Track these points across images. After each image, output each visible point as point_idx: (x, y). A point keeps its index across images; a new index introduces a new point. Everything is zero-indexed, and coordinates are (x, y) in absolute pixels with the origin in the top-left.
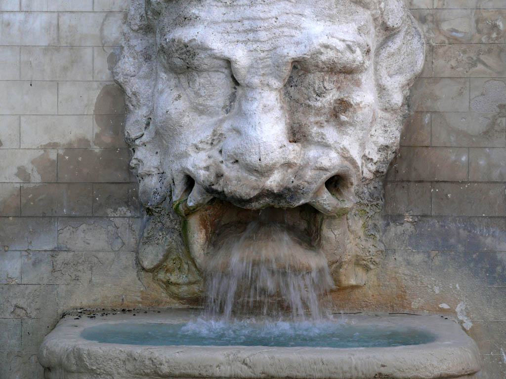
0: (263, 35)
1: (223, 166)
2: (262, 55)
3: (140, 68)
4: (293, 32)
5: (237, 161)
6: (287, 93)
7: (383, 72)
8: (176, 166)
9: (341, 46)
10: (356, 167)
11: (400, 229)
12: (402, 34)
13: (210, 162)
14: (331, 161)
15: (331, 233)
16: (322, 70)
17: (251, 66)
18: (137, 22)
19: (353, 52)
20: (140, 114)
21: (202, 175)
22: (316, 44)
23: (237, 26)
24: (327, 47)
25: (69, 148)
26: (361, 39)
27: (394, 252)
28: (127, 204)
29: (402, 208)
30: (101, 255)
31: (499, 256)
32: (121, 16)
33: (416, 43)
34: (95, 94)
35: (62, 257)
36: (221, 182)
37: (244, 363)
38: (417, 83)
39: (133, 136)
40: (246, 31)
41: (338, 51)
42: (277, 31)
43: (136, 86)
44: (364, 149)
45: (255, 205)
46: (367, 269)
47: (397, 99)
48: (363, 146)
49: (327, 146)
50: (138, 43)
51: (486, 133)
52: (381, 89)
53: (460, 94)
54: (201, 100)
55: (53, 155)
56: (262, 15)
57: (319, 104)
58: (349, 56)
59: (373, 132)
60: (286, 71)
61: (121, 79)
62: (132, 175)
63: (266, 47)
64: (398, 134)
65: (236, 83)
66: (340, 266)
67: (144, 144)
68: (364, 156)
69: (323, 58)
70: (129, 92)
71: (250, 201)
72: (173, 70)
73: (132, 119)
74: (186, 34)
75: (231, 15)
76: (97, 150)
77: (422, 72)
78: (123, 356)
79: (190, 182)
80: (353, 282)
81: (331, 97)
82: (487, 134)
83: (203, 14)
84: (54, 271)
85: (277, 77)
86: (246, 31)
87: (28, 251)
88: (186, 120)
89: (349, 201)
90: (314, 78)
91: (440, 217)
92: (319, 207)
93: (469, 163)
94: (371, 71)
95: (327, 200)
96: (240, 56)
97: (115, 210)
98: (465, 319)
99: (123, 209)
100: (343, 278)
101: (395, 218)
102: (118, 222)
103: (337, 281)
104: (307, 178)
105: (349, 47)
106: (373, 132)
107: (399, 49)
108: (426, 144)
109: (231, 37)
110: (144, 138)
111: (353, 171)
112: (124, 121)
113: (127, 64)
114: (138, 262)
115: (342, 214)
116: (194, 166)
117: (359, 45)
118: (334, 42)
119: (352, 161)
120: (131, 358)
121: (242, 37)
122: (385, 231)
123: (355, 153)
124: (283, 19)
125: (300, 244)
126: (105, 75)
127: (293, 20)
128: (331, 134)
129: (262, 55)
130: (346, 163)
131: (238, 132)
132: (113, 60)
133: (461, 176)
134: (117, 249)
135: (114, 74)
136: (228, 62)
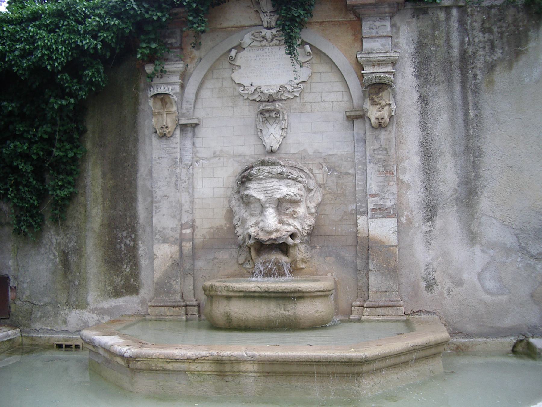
0: (269, 192)
1: (259, 232)
2: (269, 198)
3: (237, 203)
4: (278, 191)
5: (263, 230)
6: (278, 209)
7: (308, 202)
8: (246, 232)
9: (292, 194)
10: (300, 231)
11: (315, 250)
12: (314, 191)
13: (255, 230)
14: (291, 229)
15: (292, 251)
16: (287, 202)
17: (266, 201)
18: (236, 190)
19: (297, 196)
20: (237, 217)
21: (253, 234)
22: (284, 194)
23: (261, 189)
24: (287, 194)
25: (217, 228)
26: (299, 192)
27: (314, 257)
28: (234, 244)
29: (316, 244)
30: (227, 260)
31: (346, 258)
32: (232, 188)
33: (319, 194)
34: (224, 212)
35: (216, 261)
36: (258, 235)
37: (259, 287)
38: (319, 205)
39: (235, 224)
40: (264, 191)
41: (291, 196)
42: (273, 190)
43: (236, 209)
44: (302, 226)
45: (268, 243)
46: (306, 263)
47: (313, 210)
48: (302, 225)
49: (290, 225)
50: (237, 196)
51: (341, 220)
52: (308, 208)
53: (332, 208)
54: (253, 212)
55: (212, 231)
56: (269, 186)
57: (287, 212)
58: (295, 198)
59: (305, 221)
60: (277, 202)
61: (232, 207)
62: (236, 236)
63: (270, 195)
64: (314, 221)
65: (263, 207)
66: (297, 262)
67: (238, 226)
68: (303, 228)
69: (287, 198)
70: (234, 211)
71: (266, 241)
72: (244, 203)
73: (235, 219)
74: (246, 193)
75: (260, 186)
76: (225, 228)
77: (321, 202)
78: (224, 286)
79: (250, 236)
80: (301, 267)
81: (291, 210)
82: (341, 220)
83: (252, 186)
84: (213, 265)
85: (275, 205)
86: (264, 191)
87: (206, 259)
88: (248, 218)
89: (298, 241)
90: (285, 205)
91: (327, 246)
92: (288, 243)
93: (336, 230)
94: (304, 202)
95: (290, 241)
96: (262, 197)
97: (231, 246)
98: (336, 277)
99: (233, 246)
100: (298, 265)
101: (314, 247)
102: (232, 250)
103: (296, 266)
104: (283, 234)
105: (295, 195)
106: (305, 221)
107: (313, 195)
108: (323, 224)
109: (259, 193)
110: (238, 225)
111: (298, 232)
112: (233, 220)
113: (234, 203)
114: (237, 262)
115: (295, 245)
116: (251, 232)
117: (298, 194)
118: (290, 193)
119: (298, 229)
120: (226, 286)
121: (263, 193)
122: (311, 251)
123: (299, 226)
124: (275, 187)
125: (284, 255)
126: (227, 206)
127: (277, 187)
128: (291, 221)
129: (269, 198)
130: (296, 230)
131: (262, 221)
132: (229, 201)
133: (334, 234)
134: (240, 263)
135: (230, 206)
136: (259, 200)
